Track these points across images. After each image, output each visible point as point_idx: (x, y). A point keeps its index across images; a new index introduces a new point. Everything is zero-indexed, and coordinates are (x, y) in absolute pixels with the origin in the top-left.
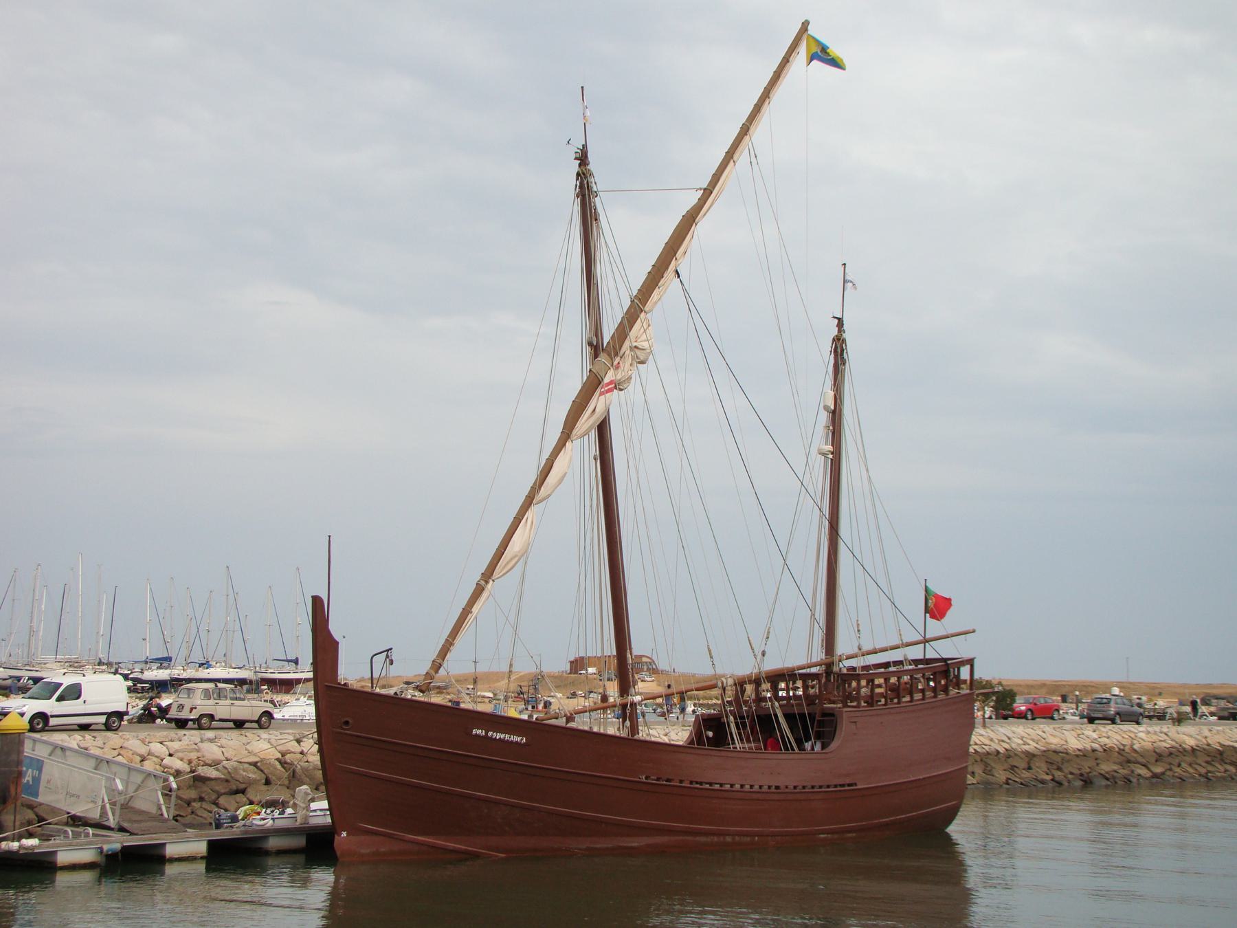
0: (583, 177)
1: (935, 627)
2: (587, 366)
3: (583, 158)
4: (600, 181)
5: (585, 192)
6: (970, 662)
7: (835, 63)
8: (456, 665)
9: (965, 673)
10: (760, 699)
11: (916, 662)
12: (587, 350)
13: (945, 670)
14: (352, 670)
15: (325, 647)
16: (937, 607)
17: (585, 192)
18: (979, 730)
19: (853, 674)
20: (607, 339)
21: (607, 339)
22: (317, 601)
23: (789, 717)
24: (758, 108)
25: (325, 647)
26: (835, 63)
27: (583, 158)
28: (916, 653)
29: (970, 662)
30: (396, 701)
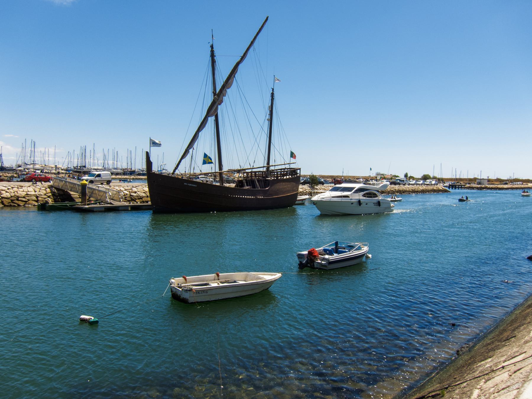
0: (212, 52)
1: (293, 160)
2: (213, 98)
3: (212, 47)
4: (216, 53)
5: (213, 55)
6: (300, 169)
7: (159, 145)
8: (177, 172)
9: (298, 171)
10: (252, 176)
11: (288, 169)
12: (213, 94)
13: (293, 172)
14: (155, 169)
15: (149, 164)
16: (293, 155)
17: (213, 55)
18: (301, 186)
19: (273, 171)
20: (217, 92)
21: (217, 92)
22: (147, 153)
23: (258, 181)
24: (255, 38)
25: (149, 164)
26: (159, 145)
27: (212, 47)
28: (287, 166)
29: (300, 169)
30: (165, 176)
